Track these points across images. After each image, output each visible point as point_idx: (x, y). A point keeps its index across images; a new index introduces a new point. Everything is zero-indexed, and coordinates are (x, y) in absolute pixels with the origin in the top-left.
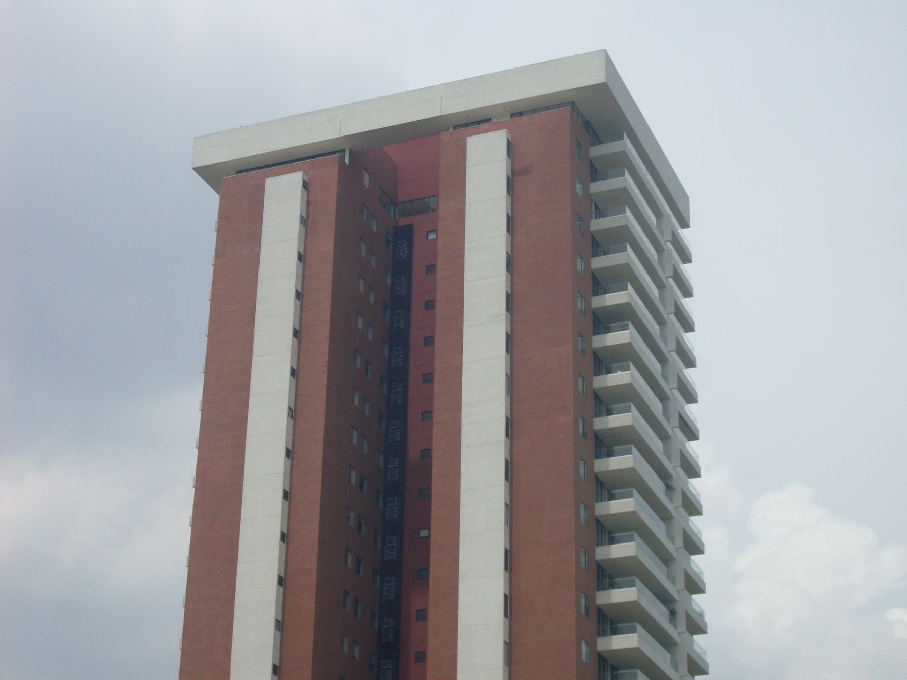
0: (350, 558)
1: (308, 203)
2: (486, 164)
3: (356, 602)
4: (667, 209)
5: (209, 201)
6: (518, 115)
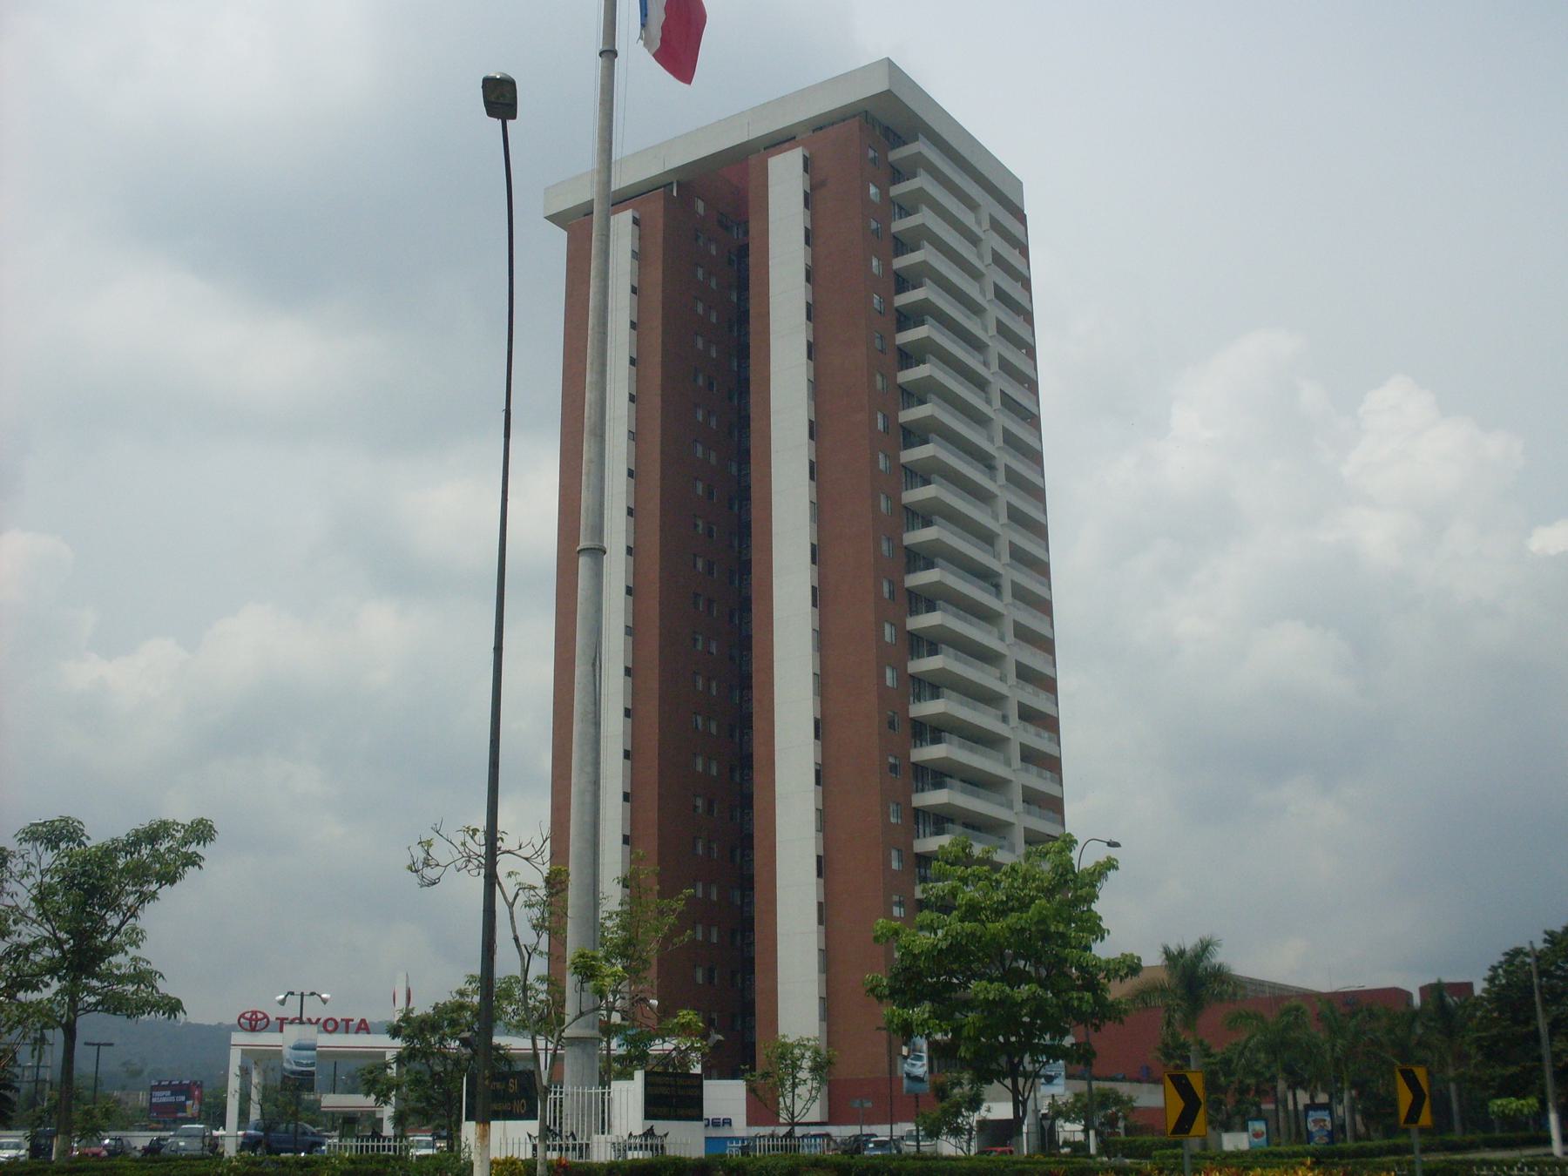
0: (700, 564)
2: (785, 179)
3: (710, 602)
4: (974, 190)
5: (561, 236)
6: (820, 125)
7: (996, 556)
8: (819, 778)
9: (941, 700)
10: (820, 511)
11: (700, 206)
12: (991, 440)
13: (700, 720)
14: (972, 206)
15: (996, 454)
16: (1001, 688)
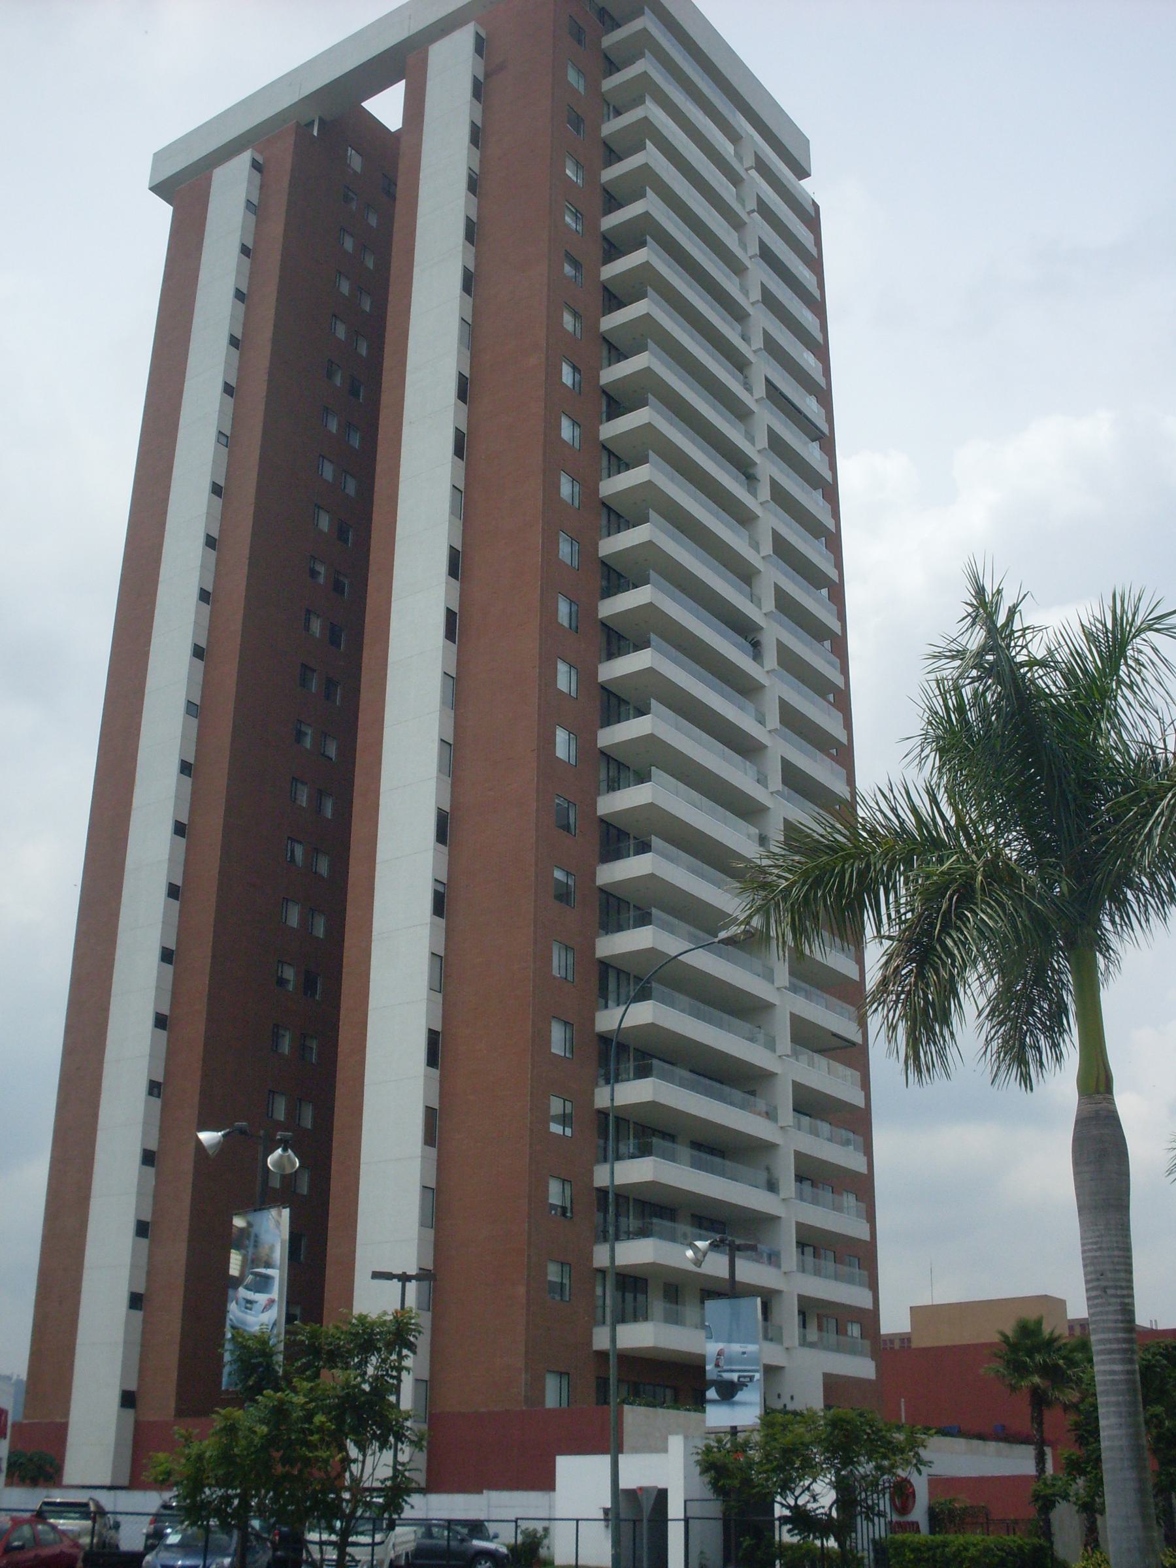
0: (316, 626)
5: (164, 212)
7: (754, 599)
8: (440, 905)
9: (647, 786)
10: (468, 502)
11: (356, 162)
12: (755, 546)
13: (299, 851)
14: (734, 137)
15: (757, 458)
16: (760, 794)
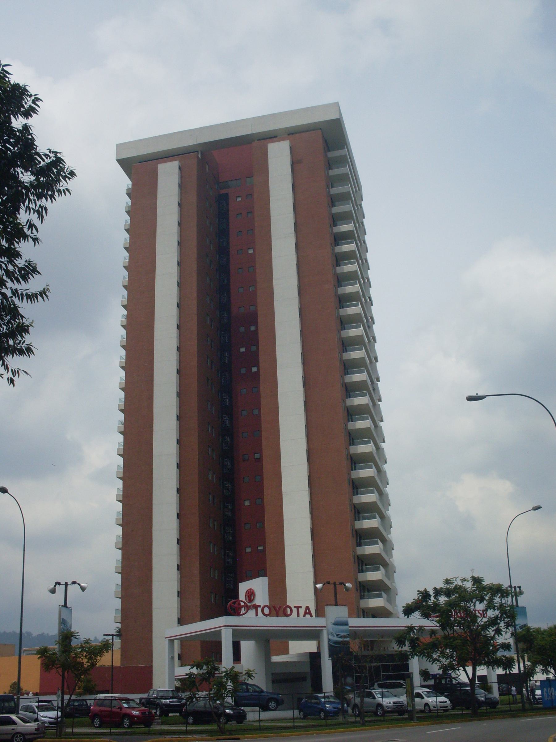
1: (181, 177)
2: (279, 158)
6: (291, 134)
